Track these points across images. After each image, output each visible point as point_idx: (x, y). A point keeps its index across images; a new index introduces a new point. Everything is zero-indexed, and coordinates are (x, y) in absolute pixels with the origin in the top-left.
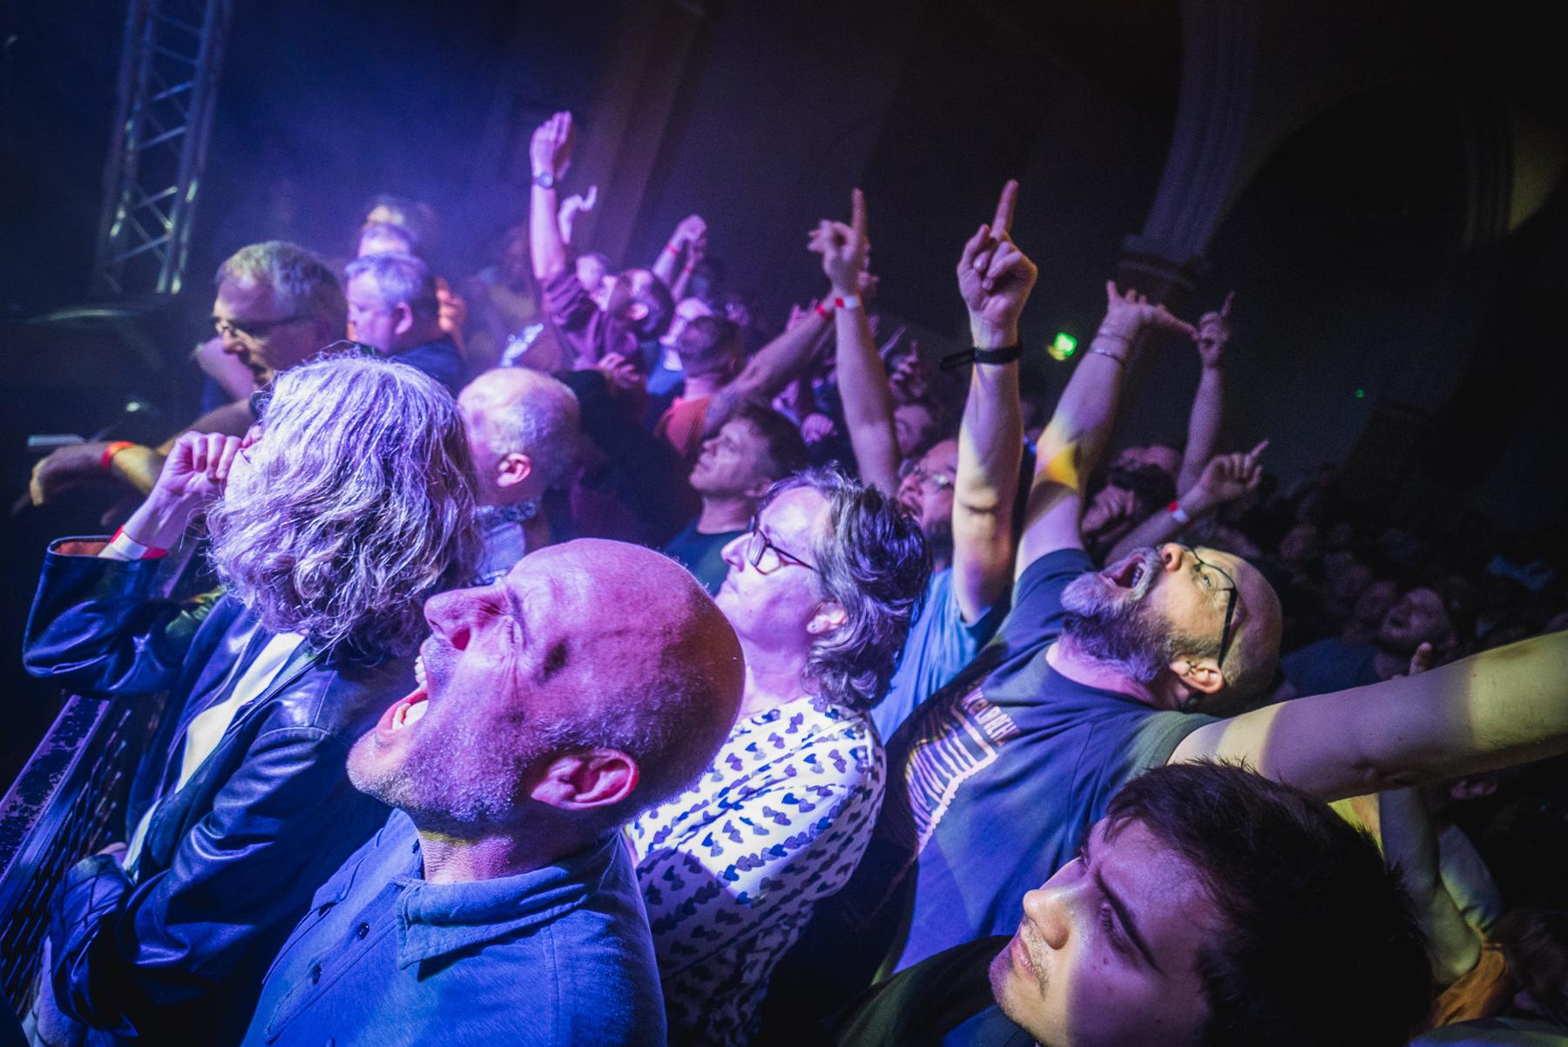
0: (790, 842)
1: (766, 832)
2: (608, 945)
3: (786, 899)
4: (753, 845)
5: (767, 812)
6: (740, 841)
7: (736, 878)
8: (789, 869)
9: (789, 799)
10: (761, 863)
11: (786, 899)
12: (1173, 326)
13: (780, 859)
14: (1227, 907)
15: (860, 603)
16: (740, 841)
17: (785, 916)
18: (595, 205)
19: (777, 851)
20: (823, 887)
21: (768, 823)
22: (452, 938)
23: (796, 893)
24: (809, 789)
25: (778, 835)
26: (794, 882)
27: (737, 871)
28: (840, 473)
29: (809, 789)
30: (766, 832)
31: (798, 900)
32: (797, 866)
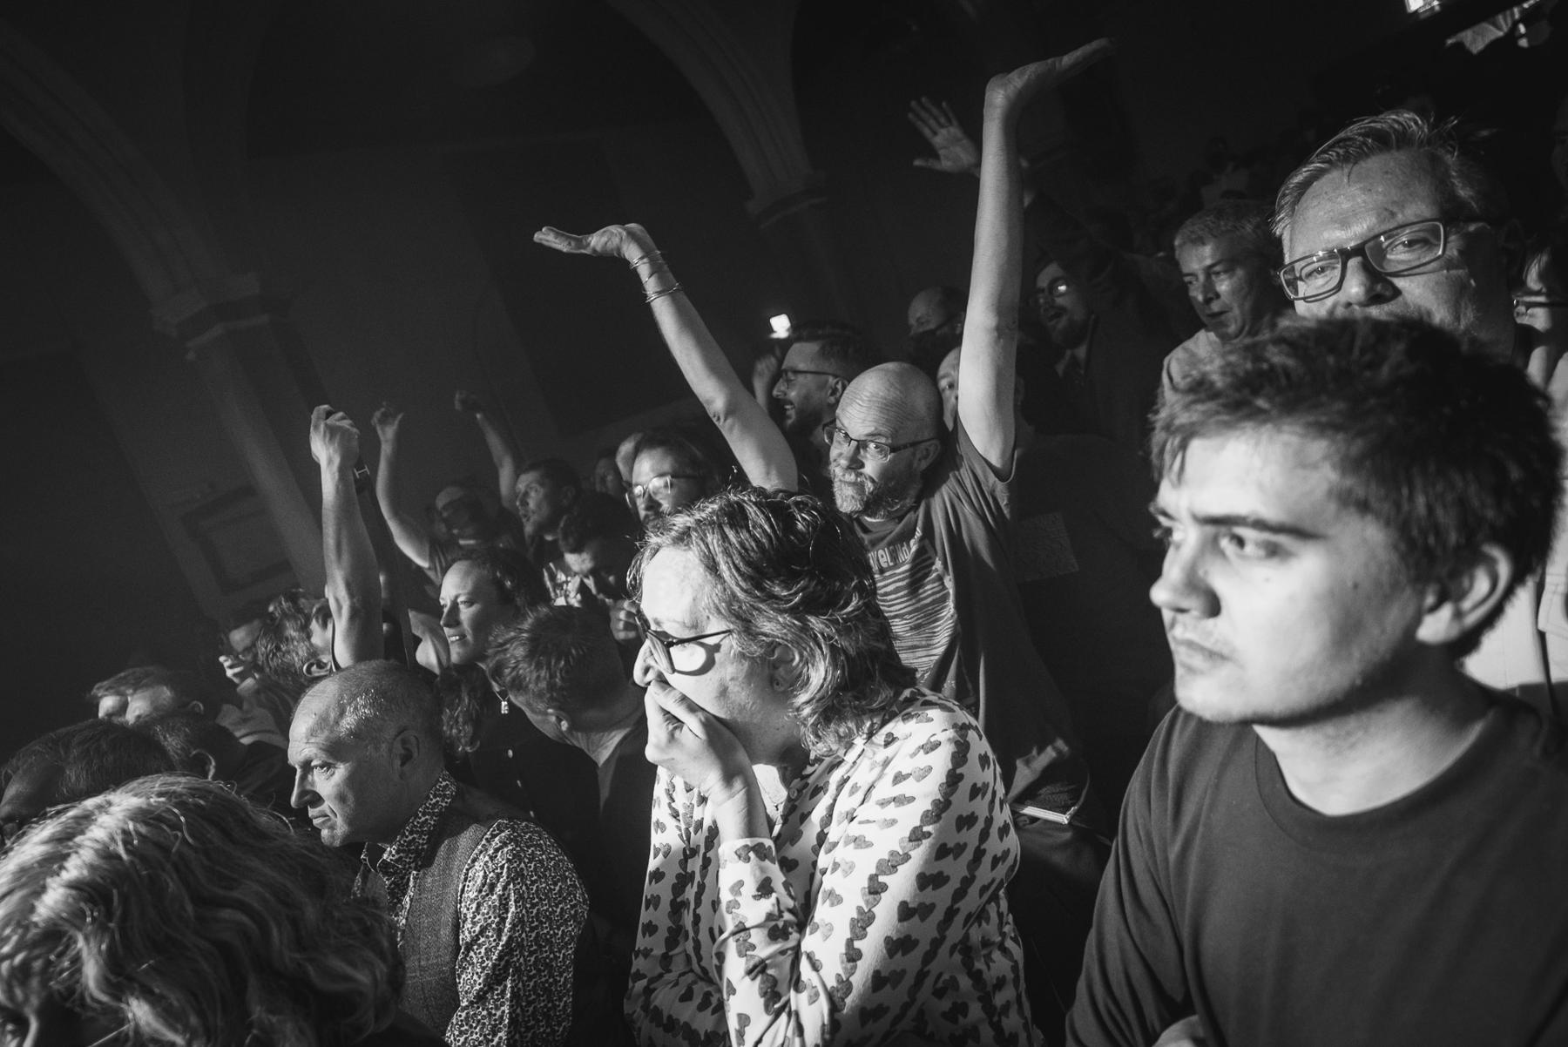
0: (927, 818)
1: (894, 822)
2: (1122, 951)
3: (960, 894)
4: (889, 841)
5: (883, 804)
6: (869, 845)
7: (884, 887)
8: (941, 852)
9: (899, 778)
10: (907, 857)
11: (960, 894)
12: (403, 523)
13: (926, 843)
14: (1321, 429)
15: (805, 628)
16: (869, 845)
17: (969, 916)
18: (867, 561)
19: (917, 836)
20: (996, 861)
21: (892, 811)
22: (1185, 933)
23: (967, 882)
24: (914, 755)
25: (910, 817)
26: (956, 869)
27: (881, 879)
28: (327, 739)
29: (914, 755)
30: (894, 822)
31: (974, 890)
32: (951, 845)
